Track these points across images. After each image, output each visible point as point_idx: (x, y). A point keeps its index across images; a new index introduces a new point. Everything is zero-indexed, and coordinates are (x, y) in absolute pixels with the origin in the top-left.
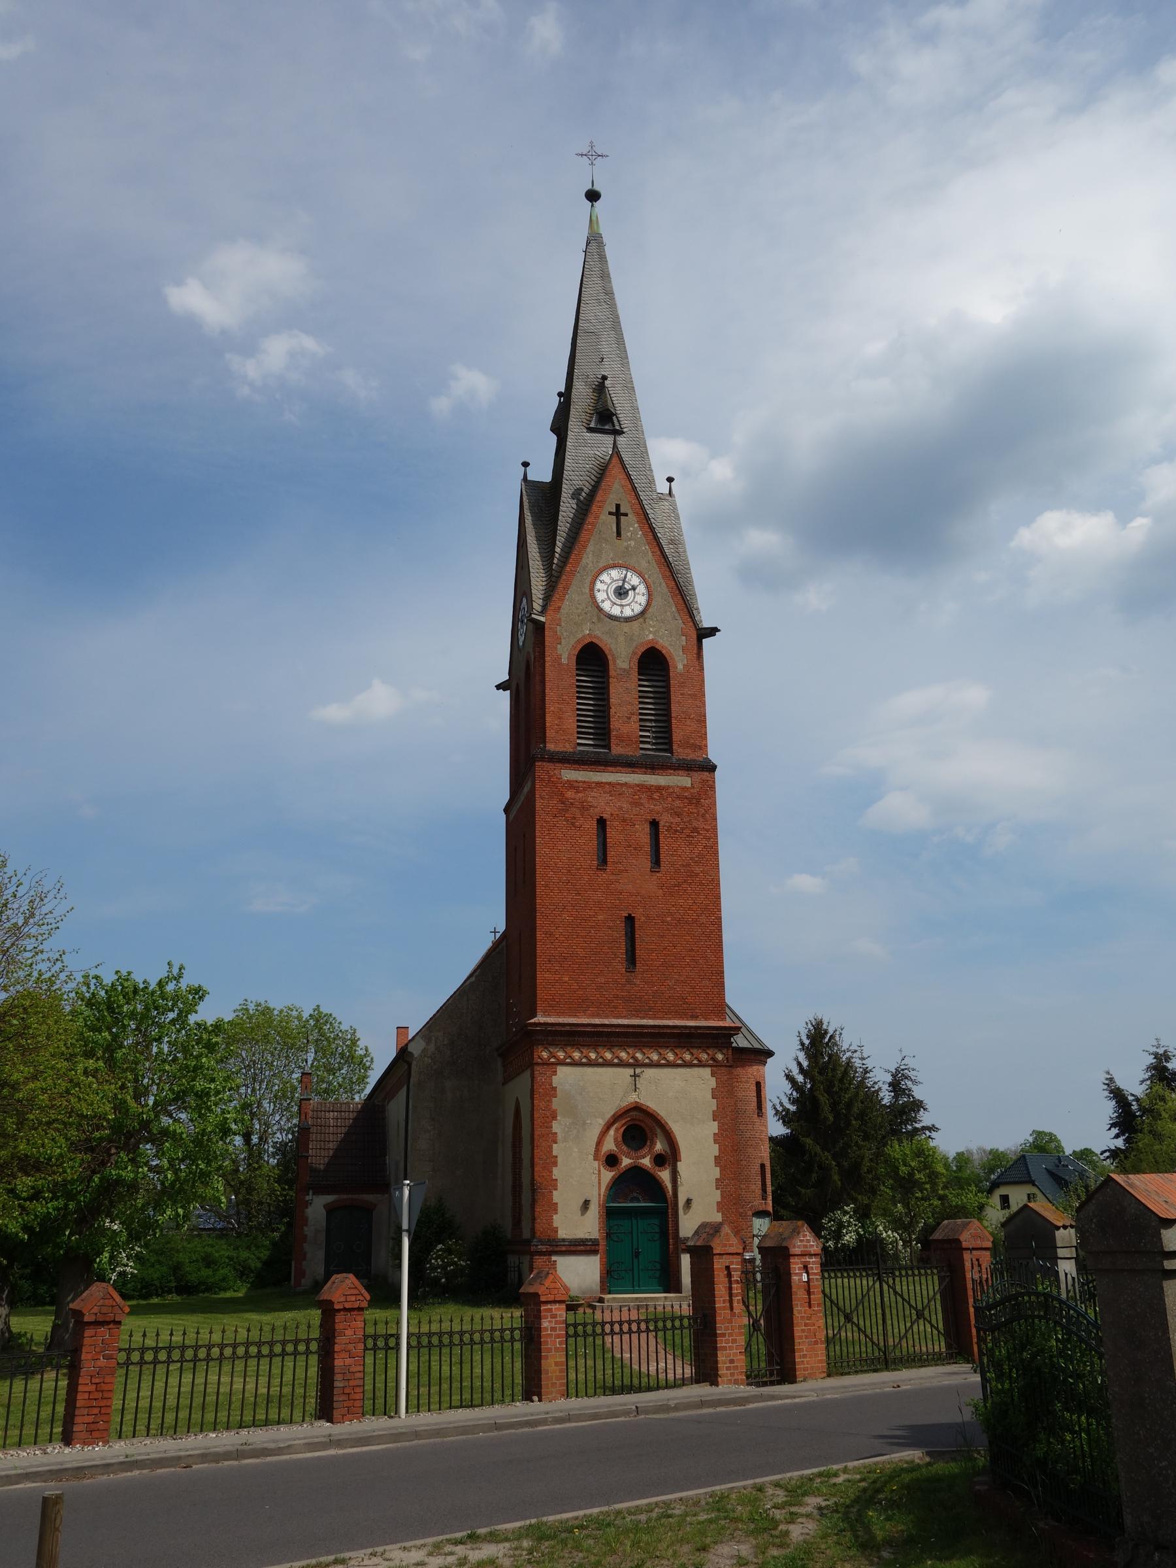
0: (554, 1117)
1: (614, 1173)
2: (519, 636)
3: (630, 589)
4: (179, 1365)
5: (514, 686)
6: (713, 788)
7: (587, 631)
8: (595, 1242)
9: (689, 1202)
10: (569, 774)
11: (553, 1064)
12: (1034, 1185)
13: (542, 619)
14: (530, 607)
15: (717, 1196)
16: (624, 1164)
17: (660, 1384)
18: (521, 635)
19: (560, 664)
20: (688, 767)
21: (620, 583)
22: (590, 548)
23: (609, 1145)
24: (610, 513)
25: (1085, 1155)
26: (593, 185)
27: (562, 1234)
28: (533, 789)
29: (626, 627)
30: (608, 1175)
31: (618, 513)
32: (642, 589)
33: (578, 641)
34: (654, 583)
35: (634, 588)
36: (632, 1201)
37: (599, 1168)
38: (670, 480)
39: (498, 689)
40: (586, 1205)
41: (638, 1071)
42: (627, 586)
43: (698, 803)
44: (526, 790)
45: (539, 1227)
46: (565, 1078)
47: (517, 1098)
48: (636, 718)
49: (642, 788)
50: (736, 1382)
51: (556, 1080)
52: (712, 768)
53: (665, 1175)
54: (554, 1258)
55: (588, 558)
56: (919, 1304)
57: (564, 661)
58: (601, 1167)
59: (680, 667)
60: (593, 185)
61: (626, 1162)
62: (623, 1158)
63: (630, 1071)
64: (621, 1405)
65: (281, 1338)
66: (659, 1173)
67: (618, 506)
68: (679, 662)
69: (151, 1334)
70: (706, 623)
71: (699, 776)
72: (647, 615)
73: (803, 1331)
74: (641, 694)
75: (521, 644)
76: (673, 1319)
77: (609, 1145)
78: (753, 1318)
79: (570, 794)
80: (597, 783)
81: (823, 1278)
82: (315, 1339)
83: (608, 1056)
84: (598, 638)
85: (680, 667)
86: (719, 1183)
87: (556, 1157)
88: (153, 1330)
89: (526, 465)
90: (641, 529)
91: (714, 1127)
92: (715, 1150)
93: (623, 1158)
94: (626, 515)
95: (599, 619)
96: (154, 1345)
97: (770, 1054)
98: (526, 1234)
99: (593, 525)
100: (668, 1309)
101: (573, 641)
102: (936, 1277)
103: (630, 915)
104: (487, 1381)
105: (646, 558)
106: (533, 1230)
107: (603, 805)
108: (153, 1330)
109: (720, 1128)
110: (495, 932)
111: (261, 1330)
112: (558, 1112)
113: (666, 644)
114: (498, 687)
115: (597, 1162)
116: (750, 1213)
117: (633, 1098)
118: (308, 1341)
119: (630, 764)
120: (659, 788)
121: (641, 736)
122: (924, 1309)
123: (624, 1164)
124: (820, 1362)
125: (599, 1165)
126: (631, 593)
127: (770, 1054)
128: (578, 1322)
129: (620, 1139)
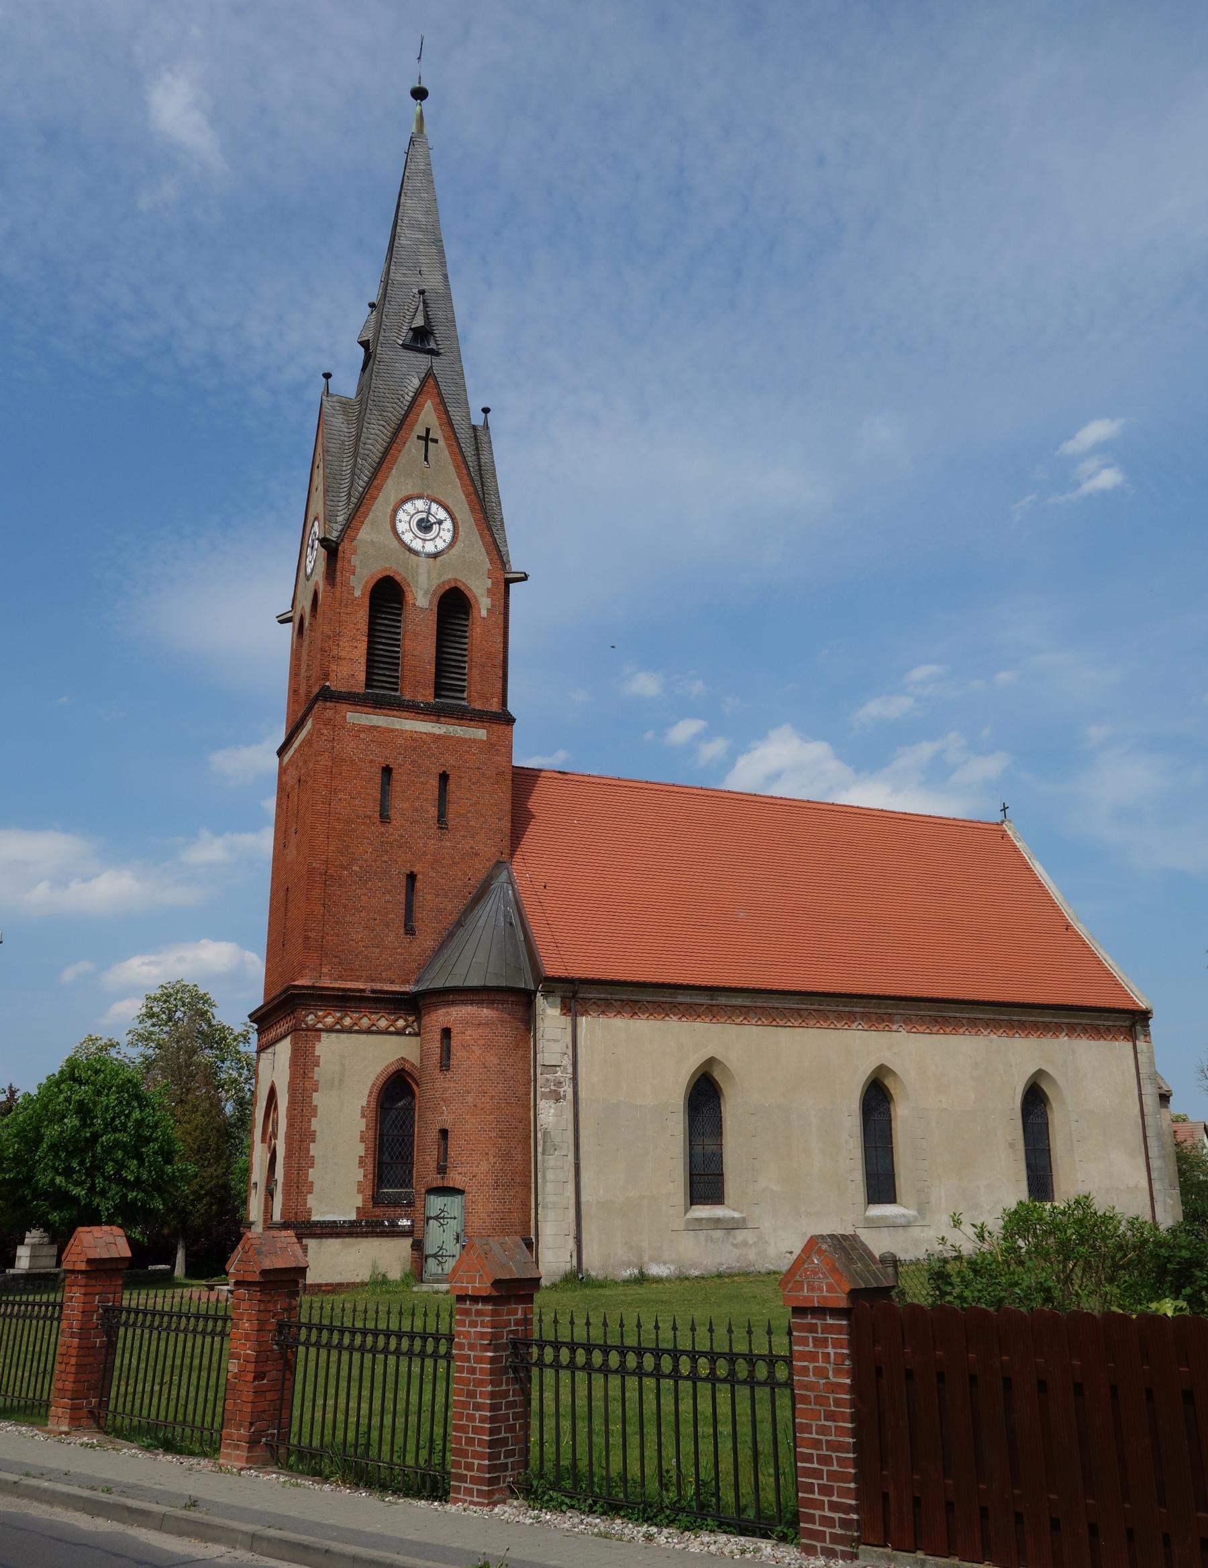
3: (435, 523)
18: (310, 562)
21: (424, 515)
24: (419, 437)
26: (420, 83)
31: (426, 438)
32: (448, 524)
35: (440, 522)
38: (486, 410)
42: (432, 520)
52: (510, 720)
55: (390, 490)
60: (420, 83)
67: (428, 430)
68: (483, 605)
71: (499, 729)
75: (309, 571)
88: (669, 1318)
89: (327, 376)
94: (436, 441)
103: (444, 772)
104: (151, 1366)
108: (669, 1318)
116: (423, 1191)
126: (436, 527)
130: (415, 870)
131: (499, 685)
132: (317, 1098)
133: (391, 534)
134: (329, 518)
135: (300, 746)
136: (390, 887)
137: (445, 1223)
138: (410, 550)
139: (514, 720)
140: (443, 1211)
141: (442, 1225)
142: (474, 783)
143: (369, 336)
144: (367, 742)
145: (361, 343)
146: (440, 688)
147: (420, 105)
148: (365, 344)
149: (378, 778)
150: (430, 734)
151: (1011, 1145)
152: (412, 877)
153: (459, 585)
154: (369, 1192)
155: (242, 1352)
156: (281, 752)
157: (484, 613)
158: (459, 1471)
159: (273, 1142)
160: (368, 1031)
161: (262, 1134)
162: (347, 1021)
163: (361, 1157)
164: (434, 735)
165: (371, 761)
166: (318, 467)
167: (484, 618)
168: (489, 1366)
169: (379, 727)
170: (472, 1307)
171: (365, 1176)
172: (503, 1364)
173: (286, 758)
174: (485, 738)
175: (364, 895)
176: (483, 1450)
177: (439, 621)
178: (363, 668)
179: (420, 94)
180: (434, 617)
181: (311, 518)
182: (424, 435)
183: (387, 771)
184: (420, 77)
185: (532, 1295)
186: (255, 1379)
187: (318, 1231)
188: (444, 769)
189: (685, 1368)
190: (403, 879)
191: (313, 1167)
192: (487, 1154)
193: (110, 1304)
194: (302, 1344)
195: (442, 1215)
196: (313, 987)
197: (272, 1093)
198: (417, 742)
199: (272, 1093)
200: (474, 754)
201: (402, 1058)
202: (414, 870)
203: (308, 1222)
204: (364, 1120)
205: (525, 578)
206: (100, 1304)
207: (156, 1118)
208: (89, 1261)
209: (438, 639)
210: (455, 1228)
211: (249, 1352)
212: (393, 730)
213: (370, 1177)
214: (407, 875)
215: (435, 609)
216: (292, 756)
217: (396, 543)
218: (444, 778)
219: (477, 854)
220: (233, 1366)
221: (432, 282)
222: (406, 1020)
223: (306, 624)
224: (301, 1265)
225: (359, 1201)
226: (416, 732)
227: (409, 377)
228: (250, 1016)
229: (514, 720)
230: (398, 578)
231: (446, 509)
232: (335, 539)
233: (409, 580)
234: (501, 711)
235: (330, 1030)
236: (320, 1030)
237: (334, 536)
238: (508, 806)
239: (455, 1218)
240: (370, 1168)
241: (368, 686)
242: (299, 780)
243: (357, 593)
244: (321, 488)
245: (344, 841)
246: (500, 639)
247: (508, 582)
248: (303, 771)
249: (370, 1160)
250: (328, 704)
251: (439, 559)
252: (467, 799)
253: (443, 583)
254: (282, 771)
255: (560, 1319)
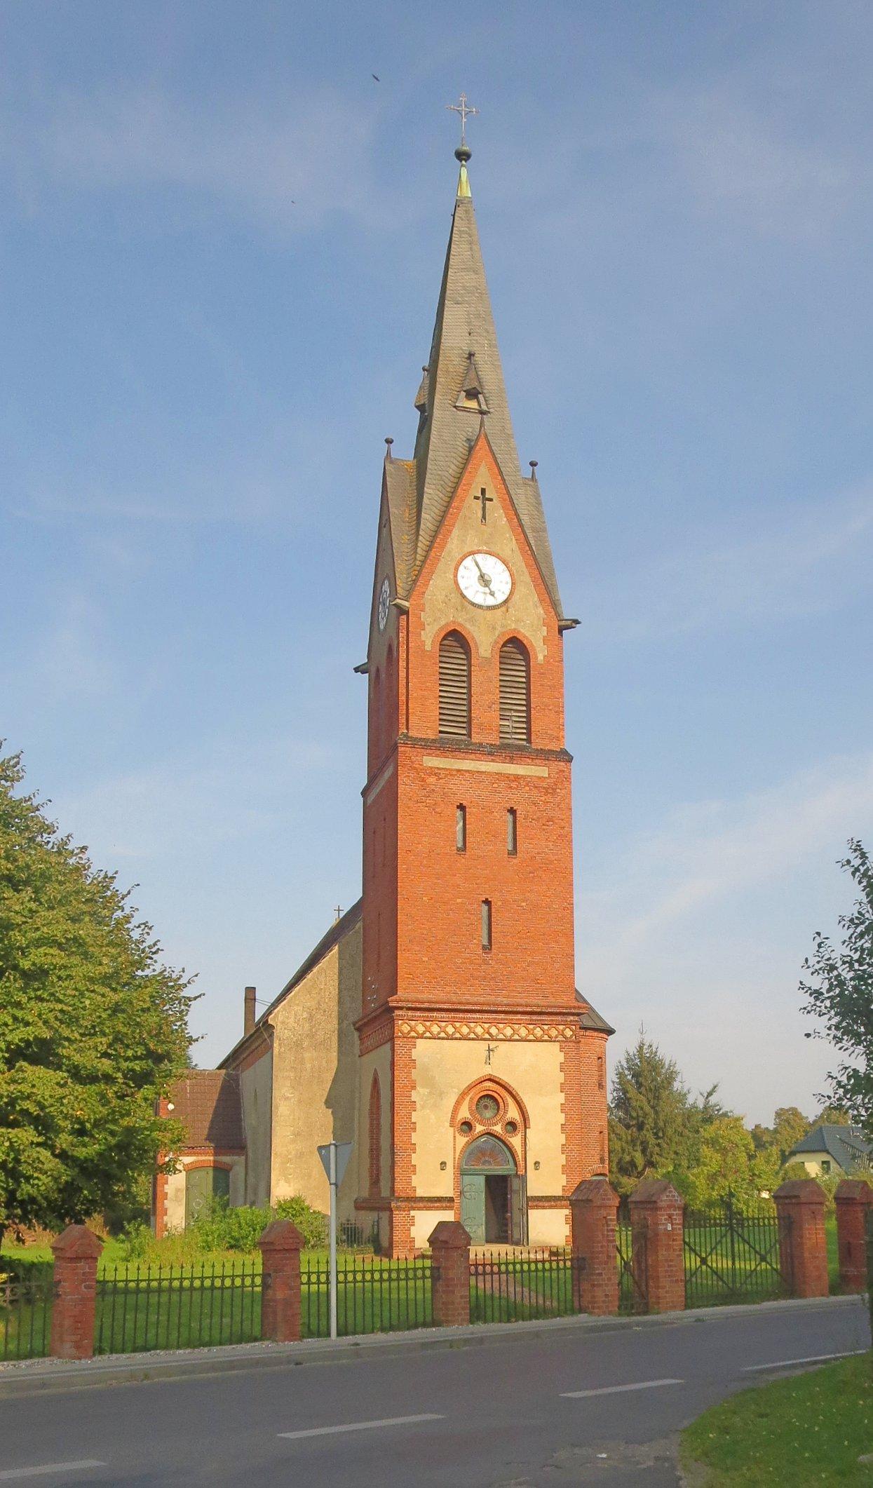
0: (414, 1088)
1: (468, 1138)
5: (373, 669)
6: (568, 779)
8: (451, 1200)
9: (537, 1163)
10: (432, 761)
11: (413, 1037)
12: (828, 1153)
13: (406, 604)
14: (394, 586)
15: (562, 1159)
16: (477, 1131)
17: (357, 1330)
19: (424, 651)
20: (545, 755)
22: (455, 532)
23: (464, 1113)
25: (682, 1097)
28: (395, 775)
29: (489, 614)
30: (462, 1140)
31: (483, 497)
33: (441, 629)
34: (517, 572)
36: (483, 1164)
37: (454, 1134)
39: (356, 672)
40: (443, 1164)
41: (493, 1044)
43: (554, 792)
44: (387, 774)
45: (398, 1186)
46: (423, 1050)
47: (375, 1070)
48: (496, 707)
49: (500, 776)
50: (610, 1313)
51: (415, 1054)
52: (570, 759)
53: (516, 1141)
54: (412, 1213)
55: (454, 544)
56: (763, 1250)
57: (428, 647)
58: (457, 1132)
59: (541, 657)
61: (479, 1128)
62: (477, 1125)
63: (483, 1046)
65: (240, 1273)
66: (509, 1139)
67: (483, 491)
68: (540, 653)
69: (313, 1263)
70: (568, 614)
72: (510, 604)
73: (666, 1271)
74: (502, 684)
75: (382, 627)
76: (492, 1265)
77: (464, 1113)
78: (624, 1260)
79: (432, 780)
80: (459, 771)
81: (684, 1227)
82: (259, 1275)
83: (465, 1030)
84: (461, 625)
85: (541, 657)
86: (564, 1148)
87: (415, 1123)
90: (507, 515)
91: (561, 1098)
92: (561, 1118)
93: (477, 1125)
94: (491, 500)
95: (463, 607)
96: (251, 1273)
97: (610, 1032)
98: (385, 1193)
99: (459, 509)
100: (503, 1255)
101: (436, 627)
105: (510, 545)
106: (393, 1190)
107: (462, 791)
109: (566, 1099)
110: (339, 910)
111: (224, 1266)
112: (417, 1082)
113: (527, 634)
114: (357, 670)
115: (452, 1129)
117: (488, 1071)
118: (253, 1276)
119: (492, 752)
120: (517, 778)
121: (440, 696)
122: (707, 1256)
123: (477, 1131)
124: (680, 1296)
125: (454, 1132)
127: (610, 1032)
128: (195, 1276)
129: (474, 1108)
143: (424, 400)
145: (417, 407)
148: (420, 408)
156: (365, 793)
189: (402, 1276)
223: (383, 676)
235: (421, 1037)
255: (226, 1265)
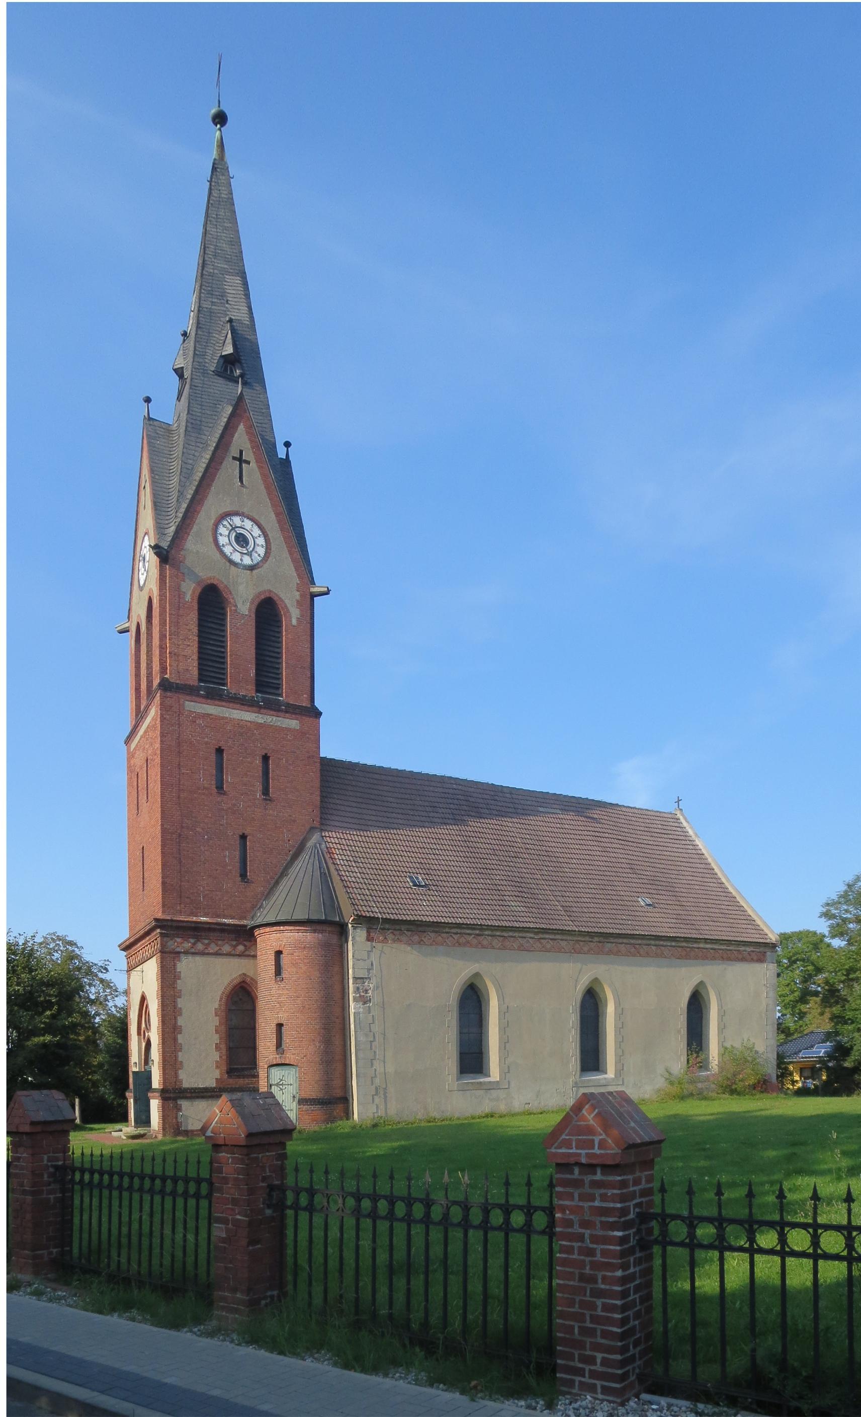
2: (140, 576)
4: (685, 1213)
7: (206, 574)
18: (143, 574)
24: (234, 458)
27: (186, 1085)
28: (147, 1002)
38: (287, 444)
52: (318, 714)
54: (179, 1102)
64: (709, 1115)
67: (241, 452)
68: (293, 615)
71: (308, 720)
75: (142, 583)
89: (148, 400)
94: (248, 463)
102: (76, 1251)
103: (266, 754)
130: (246, 833)
131: (308, 683)
132: (180, 1003)
133: (213, 546)
134: (160, 528)
135: (146, 732)
136: (227, 845)
137: (284, 1088)
138: (231, 562)
139: (320, 714)
140: (282, 1080)
141: (282, 1089)
142: (290, 764)
144: (203, 727)
146: (260, 686)
147: (220, 129)
149: (213, 757)
150: (254, 722)
151: (679, 1032)
152: (243, 837)
153: (272, 595)
154: (224, 1068)
155: (230, 1218)
156: (128, 741)
157: (294, 622)
158: (572, 1364)
159: (147, 1034)
160: (217, 954)
161: (138, 1029)
162: (200, 946)
163: (217, 1044)
164: (257, 723)
165: (206, 743)
166: (144, 487)
167: (294, 626)
168: (618, 1248)
169: (211, 715)
170: (585, 1178)
171: (220, 1057)
172: (631, 1244)
173: (133, 746)
174: (298, 728)
175: (207, 850)
176: (612, 1343)
177: (257, 627)
178: (196, 664)
179: (220, 119)
180: (253, 623)
181: (140, 534)
182: (238, 456)
183: (220, 751)
184: (219, 101)
185: (652, 1161)
186: (249, 1244)
187: (189, 1095)
188: (266, 752)
190: (237, 837)
191: (181, 1051)
192: (314, 1040)
193: (60, 1163)
194: (291, 1207)
195: (281, 1083)
196: (172, 920)
197: (143, 999)
198: (243, 729)
199: (143, 999)
200: (289, 740)
201: (244, 974)
202: (245, 832)
203: (180, 1089)
204: (217, 1018)
205: (327, 593)
206: (49, 1164)
207: (88, 987)
208: (33, 1123)
209: (257, 643)
210: (292, 1091)
211: (239, 1217)
212: (223, 718)
213: (224, 1057)
214: (240, 835)
215: (253, 616)
216: (139, 742)
217: (218, 555)
218: (266, 758)
219: (294, 821)
220: (219, 1231)
221: (239, 313)
222: (245, 946)
224: (289, 1127)
225: (217, 1074)
226: (242, 720)
227: (222, 403)
228: (119, 946)
229: (320, 714)
230: (221, 587)
231: (260, 527)
232: (166, 548)
233: (231, 588)
234: (309, 706)
235: (186, 953)
236: (179, 953)
237: (165, 545)
238: (317, 783)
239: (291, 1085)
240: (224, 1052)
241: (200, 680)
242: (147, 760)
243: (188, 598)
244: (149, 504)
245: (188, 807)
246: (308, 645)
247: (313, 596)
248: (150, 752)
249: (223, 1046)
250: (169, 694)
251: (255, 572)
252: (285, 777)
253: (260, 594)
254: (131, 756)
